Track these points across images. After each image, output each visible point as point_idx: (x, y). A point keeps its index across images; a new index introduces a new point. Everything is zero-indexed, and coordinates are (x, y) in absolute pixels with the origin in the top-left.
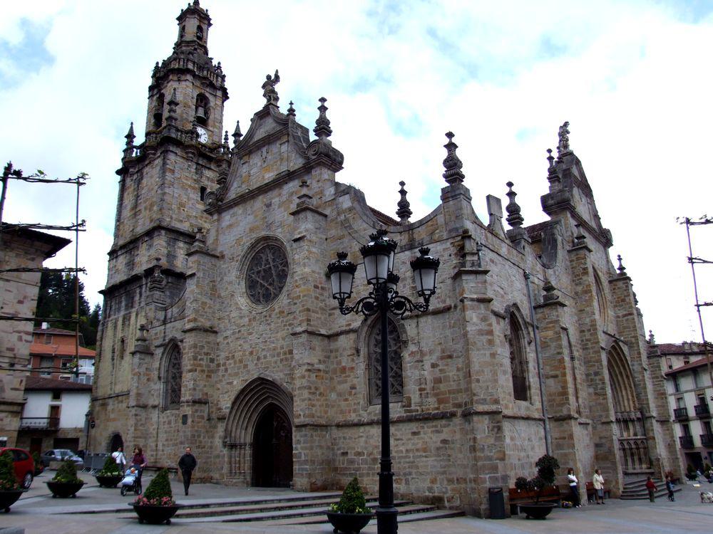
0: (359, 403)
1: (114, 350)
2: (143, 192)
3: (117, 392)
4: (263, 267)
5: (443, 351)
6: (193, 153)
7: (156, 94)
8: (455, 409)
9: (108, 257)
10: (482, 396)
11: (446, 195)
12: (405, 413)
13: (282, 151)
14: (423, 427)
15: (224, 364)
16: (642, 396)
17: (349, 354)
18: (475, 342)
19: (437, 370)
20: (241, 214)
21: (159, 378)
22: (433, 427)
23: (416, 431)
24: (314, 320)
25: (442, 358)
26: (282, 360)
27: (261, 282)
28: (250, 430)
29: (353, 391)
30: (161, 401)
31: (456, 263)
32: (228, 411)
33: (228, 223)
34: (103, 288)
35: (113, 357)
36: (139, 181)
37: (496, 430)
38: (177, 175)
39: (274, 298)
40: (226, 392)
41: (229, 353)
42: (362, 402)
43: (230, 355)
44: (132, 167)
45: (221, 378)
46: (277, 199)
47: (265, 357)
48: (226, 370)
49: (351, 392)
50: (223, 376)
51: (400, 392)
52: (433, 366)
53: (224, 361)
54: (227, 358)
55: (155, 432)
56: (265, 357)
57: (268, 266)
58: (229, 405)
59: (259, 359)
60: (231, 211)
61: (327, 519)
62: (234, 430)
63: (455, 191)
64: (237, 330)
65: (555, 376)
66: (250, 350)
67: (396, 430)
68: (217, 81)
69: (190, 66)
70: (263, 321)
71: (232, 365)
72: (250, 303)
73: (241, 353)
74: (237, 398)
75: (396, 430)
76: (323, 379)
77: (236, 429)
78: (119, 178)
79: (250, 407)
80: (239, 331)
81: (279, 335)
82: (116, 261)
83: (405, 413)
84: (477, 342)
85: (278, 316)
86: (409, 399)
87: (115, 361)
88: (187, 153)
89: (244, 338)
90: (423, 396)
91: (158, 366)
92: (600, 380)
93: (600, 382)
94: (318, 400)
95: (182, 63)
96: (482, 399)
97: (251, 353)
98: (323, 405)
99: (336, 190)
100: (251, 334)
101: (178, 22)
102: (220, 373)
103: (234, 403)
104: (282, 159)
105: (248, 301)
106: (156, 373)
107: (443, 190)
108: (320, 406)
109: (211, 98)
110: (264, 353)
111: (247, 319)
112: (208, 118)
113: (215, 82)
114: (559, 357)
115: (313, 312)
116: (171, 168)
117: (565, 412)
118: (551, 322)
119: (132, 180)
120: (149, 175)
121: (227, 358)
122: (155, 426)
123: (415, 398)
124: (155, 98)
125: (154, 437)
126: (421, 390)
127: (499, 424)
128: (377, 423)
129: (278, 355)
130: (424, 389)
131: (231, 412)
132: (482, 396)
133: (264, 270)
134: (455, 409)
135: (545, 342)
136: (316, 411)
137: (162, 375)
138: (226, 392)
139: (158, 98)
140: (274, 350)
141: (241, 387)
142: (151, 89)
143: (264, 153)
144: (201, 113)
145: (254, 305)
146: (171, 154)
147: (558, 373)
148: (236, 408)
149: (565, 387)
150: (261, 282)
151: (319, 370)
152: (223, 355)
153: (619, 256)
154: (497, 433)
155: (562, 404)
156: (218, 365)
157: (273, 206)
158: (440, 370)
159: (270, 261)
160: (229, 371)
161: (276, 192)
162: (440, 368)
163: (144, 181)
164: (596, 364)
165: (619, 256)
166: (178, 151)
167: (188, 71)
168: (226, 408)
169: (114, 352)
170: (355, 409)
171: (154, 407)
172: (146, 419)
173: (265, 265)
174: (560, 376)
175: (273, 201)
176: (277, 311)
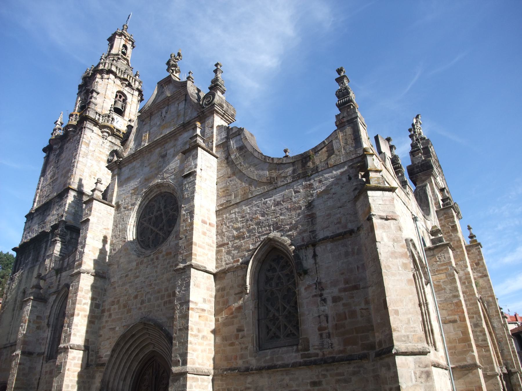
0: (246, 348)
1: (16, 300)
2: (62, 162)
3: (11, 342)
4: (155, 213)
5: (347, 282)
6: (107, 132)
7: (84, 90)
8: (366, 351)
9: (26, 219)
10: (403, 331)
11: (340, 124)
12: (302, 358)
13: (179, 109)
14: (325, 376)
15: (109, 310)
16: (505, 351)
17: (237, 292)
18: (388, 266)
19: (340, 303)
20: (139, 167)
21: (48, 325)
22: (338, 374)
23: (317, 380)
24: (200, 256)
25: (345, 290)
26: (165, 303)
27: (152, 228)
28: (129, 380)
29: (241, 334)
30: (46, 350)
31: (356, 185)
32: (107, 358)
33: (126, 177)
34: (17, 246)
35: (14, 307)
36: (59, 155)
37: (424, 376)
38: (91, 148)
39: (163, 242)
40: (108, 339)
41: (115, 298)
42: (250, 346)
43: (116, 300)
44: (56, 144)
45: (104, 324)
46: (172, 150)
47: (149, 300)
48: (110, 315)
49: (238, 335)
50: (107, 322)
51: (294, 334)
52: (335, 300)
53: (109, 307)
54: (113, 303)
55: (36, 383)
56: (149, 300)
57: (159, 212)
58: (109, 353)
59: (142, 302)
60: (130, 166)
61: (370, 173)
62: (112, 380)
63: (351, 115)
64: (125, 275)
65: (454, 321)
66: (136, 294)
67: (290, 380)
68: (135, 84)
69: (114, 69)
70: (150, 264)
71: (116, 311)
72: (140, 248)
73: (126, 297)
74: (117, 344)
75: (290, 380)
76: (207, 320)
77: (114, 380)
78: (45, 155)
79: (131, 354)
80: (127, 276)
81: (165, 276)
82: (31, 222)
83: (302, 358)
84: (391, 265)
85: (165, 257)
86: (307, 340)
87: (15, 312)
88: (102, 132)
89: (131, 282)
90: (324, 336)
91: (49, 314)
92: (481, 331)
93: (481, 334)
94: (200, 344)
95: (107, 66)
96: (404, 336)
97: (136, 297)
98: (205, 351)
99: (228, 133)
100: (137, 277)
101: (108, 42)
102: (104, 319)
103: (113, 351)
104: (178, 116)
105: (138, 246)
106: (46, 321)
107: (337, 116)
108: (202, 351)
109: (129, 96)
110: (149, 296)
111: (135, 264)
112: (124, 110)
113: (133, 84)
114: (455, 300)
115: (199, 247)
116: (87, 142)
117: (469, 361)
118: (442, 265)
119: (54, 155)
120: (68, 149)
121: (113, 303)
122: (38, 377)
123: (314, 340)
124: (82, 93)
125: (34, 388)
126: (320, 329)
127: (427, 369)
128: (371, 171)
129: (162, 297)
130: (325, 328)
131: (110, 361)
132: (403, 331)
133: (156, 217)
134: (366, 351)
135: (439, 285)
136: (197, 357)
137: (51, 323)
138: (108, 339)
139: (85, 93)
140: (159, 292)
141: (122, 333)
142: (80, 87)
143: (164, 113)
144: (119, 106)
145: (143, 250)
146: (89, 130)
147: (457, 317)
148: (115, 356)
149: (465, 332)
150: (152, 228)
151: (203, 310)
152: (110, 300)
153: (468, 226)
154: (427, 381)
155: (465, 351)
156: (103, 311)
157: (168, 156)
158: (344, 305)
159: (162, 207)
160: (113, 317)
161: (171, 144)
162: (344, 301)
163: (63, 155)
164: (475, 316)
165: (468, 226)
166: (96, 129)
167: (109, 72)
168: (106, 356)
169: (15, 304)
170: (242, 354)
171: (39, 354)
172: (30, 368)
173: (157, 211)
174: (458, 321)
175: (168, 152)
176: (164, 253)
